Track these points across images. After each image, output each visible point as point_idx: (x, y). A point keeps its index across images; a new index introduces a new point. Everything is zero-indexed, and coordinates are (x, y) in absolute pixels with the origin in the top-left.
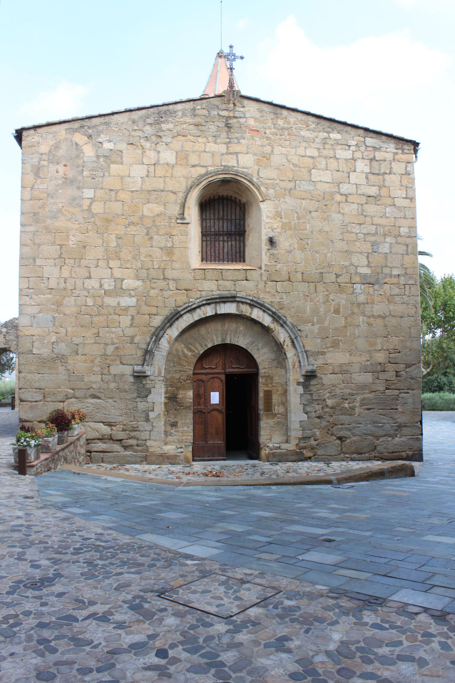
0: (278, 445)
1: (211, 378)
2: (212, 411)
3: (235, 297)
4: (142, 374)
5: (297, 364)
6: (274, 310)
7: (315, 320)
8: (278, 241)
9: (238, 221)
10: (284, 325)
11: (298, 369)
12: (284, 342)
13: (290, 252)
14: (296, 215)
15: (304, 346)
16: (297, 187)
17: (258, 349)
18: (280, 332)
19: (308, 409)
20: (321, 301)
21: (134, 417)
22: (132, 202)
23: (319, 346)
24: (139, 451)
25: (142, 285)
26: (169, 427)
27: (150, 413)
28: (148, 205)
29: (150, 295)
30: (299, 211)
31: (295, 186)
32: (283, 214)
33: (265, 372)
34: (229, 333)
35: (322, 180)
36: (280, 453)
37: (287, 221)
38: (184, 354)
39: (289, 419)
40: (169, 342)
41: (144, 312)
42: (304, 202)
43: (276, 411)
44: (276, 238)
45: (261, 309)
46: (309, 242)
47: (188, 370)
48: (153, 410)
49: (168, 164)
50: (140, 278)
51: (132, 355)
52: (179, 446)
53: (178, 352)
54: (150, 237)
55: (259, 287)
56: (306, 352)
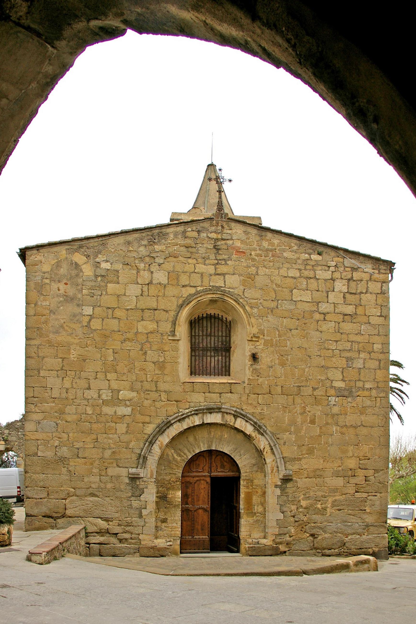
0: (257, 541)
3: (220, 408)
4: (136, 476)
5: (275, 469)
6: (255, 420)
7: (292, 429)
8: (260, 358)
10: (264, 434)
11: (277, 474)
12: (264, 449)
14: (277, 333)
15: (281, 452)
16: (279, 306)
17: (241, 455)
18: (261, 440)
19: (285, 509)
20: (298, 412)
21: (129, 514)
22: (127, 319)
23: (295, 453)
24: (133, 544)
25: (137, 396)
26: (160, 523)
31: (278, 305)
32: (265, 332)
34: (215, 440)
37: (269, 338)
38: (174, 458)
39: (267, 518)
40: (160, 448)
42: (285, 320)
43: (255, 511)
46: (289, 358)
47: (177, 473)
51: (127, 459)
52: (168, 540)
56: (283, 458)
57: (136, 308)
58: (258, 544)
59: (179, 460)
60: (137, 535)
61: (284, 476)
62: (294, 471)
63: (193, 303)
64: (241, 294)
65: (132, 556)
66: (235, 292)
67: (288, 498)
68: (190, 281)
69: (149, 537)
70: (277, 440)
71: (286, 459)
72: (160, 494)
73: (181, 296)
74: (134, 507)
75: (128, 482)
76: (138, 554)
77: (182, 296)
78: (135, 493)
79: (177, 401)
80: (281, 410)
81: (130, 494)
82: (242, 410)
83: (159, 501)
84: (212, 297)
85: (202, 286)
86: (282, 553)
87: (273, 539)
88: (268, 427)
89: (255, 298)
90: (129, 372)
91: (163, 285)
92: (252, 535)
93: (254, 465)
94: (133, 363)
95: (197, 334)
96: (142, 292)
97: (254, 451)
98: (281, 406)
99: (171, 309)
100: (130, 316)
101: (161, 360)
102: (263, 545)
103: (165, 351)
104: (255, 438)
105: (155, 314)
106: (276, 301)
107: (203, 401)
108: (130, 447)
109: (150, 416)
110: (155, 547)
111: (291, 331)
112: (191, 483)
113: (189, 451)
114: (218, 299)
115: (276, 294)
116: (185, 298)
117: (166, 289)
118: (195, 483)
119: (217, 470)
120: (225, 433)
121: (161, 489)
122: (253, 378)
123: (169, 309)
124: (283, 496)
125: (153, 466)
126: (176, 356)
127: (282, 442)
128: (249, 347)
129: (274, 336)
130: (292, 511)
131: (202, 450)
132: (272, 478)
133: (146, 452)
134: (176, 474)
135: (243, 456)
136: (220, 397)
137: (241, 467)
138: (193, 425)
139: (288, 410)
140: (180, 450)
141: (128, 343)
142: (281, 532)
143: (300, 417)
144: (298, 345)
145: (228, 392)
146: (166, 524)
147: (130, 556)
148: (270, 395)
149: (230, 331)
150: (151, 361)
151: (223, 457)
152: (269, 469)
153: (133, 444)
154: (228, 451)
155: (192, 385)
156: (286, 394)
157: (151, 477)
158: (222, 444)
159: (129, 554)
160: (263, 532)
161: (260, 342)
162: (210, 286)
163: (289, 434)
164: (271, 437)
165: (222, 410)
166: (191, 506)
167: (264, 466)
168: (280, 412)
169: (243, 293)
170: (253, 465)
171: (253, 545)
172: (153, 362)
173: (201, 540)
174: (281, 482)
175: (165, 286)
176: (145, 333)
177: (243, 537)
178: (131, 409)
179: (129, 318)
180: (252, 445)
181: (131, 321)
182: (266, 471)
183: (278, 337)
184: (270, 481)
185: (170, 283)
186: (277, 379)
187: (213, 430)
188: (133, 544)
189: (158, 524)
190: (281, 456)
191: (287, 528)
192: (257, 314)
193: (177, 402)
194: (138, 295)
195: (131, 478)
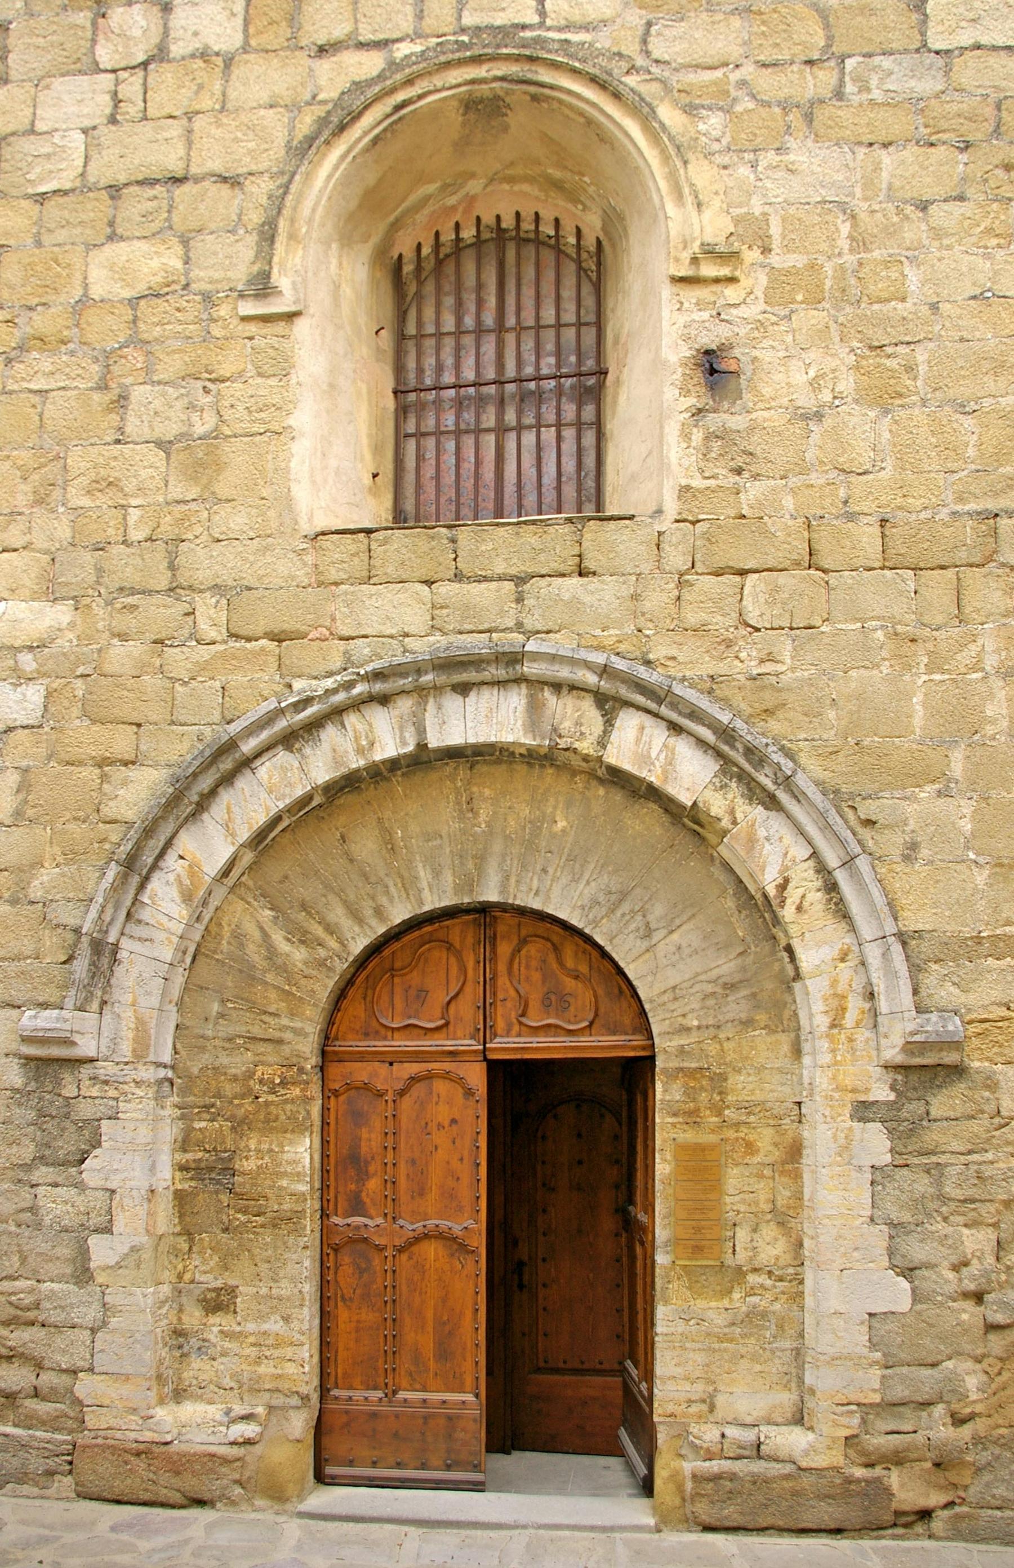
0: (749, 1436)
1: (414, 1080)
2: (417, 1240)
3: (514, 658)
4: (56, 1052)
5: (855, 1005)
6: (725, 718)
7: (957, 767)
8: (748, 369)
9: (569, 335)
10: (783, 796)
11: (864, 1035)
12: (783, 887)
13: (819, 416)
14: (845, 229)
15: (891, 905)
16: (850, 88)
17: (648, 932)
18: (762, 833)
19: (917, 1251)
20: (990, 662)
21: (23, 1260)
22: (39, 244)
23: (981, 905)
24: (43, 1423)
25: (72, 625)
26: (198, 1313)
27: (93, 1241)
28: (110, 250)
29: (108, 668)
30: (861, 207)
31: (841, 83)
32: (775, 229)
33: (681, 1051)
34: (497, 847)
35: (984, 40)
36: (756, 1480)
37: (797, 260)
38: (271, 952)
39: (809, 1301)
40: (187, 897)
41: (75, 752)
42: (886, 158)
43: (742, 1257)
44: (737, 352)
45: (656, 715)
46: (921, 356)
47: (288, 1036)
48: (107, 1229)
49: (204, 55)
50: (64, 592)
51: (18, 958)
52: (239, 1409)
53: (242, 946)
54: (113, 395)
55: (647, 606)
56: (902, 938)
57: (84, 187)
58: (760, 1457)
59: (300, 965)
60: (64, 1377)
61: (909, 1048)
62: (974, 1016)
63: (368, 120)
64: (631, 48)
65: (36, 1491)
66: (598, 45)
67: (939, 1183)
68: (356, 21)
69: (125, 1390)
70: (859, 829)
71: (925, 948)
72: (200, 1155)
73: (308, 97)
74: (47, 1221)
75: (18, 1082)
76: (68, 1480)
77: (314, 97)
78: (54, 1144)
79: (278, 638)
80: (884, 653)
81: (27, 1151)
82: (648, 663)
83: (193, 1193)
84: (468, 77)
85: (418, 35)
86: (904, 1520)
87: (848, 1432)
88: (803, 759)
89: (709, 61)
90: (40, 501)
91: (219, 61)
92: (720, 1400)
93: (731, 987)
94: (58, 457)
95: (430, 329)
96: (116, 106)
97: (730, 903)
98: (880, 634)
99: (254, 168)
100: (52, 226)
101: (199, 430)
102: (789, 1468)
103: (223, 381)
104: (725, 823)
105: (177, 200)
106: (832, 63)
107: (423, 629)
108: (32, 896)
109: (139, 725)
110: (156, 1449)
111: (924, 209)
112: (380, 1094)
113: (359, 920)
114: (505, 85)
115: (827, 26)
116: (330, 106)
117: (233, 77)
118: (402, 1093)
119: (521, 1023)
120: (555, 808)
121: (203, 1124)
122: (712, 482)
123: (245, 170)
124: (905, 1171)
125: (148, 993)
126: (276, 399)
127: (892, 843)
128: (682, 319)
129: (824, 247)
130: (966, 1264)
131: (427, 908)
132: (836, 1063)
133: (107, 918)
134: (280, 1042)
135: (662, 933)
136: (520, 600)
137: (651, 1001)
138: (362, 763)
139: (929, 654)
140: (304, 907)
141: (42, 361)
142: (900, 1392)
143: (1001, 695)
144: (974, 284)
145: (563, 568)
146: (230, 1316)
147: (26, 1489)
148: (812, 572)
149: (598, 288)
150: (148, 437)
151: (556, 948)
152: (818, 1007)
153: (45, 878)
154: (574, 908)
155: (364, 547)
156: (910, 561)
157: (140, 1055)
158: (539, 867)
159: (22, 1478)
160: (786, 1387)
161: (745, 282)
162: (463, 30)
163: (939, 793)
164: (823, 815)
165: (529, 669)
166: (380, 1220)
167: (790, 989)
168: (877, 666)
169: (645, 42)
170: (725, 986)
171: (727, 1465)
172: (159, 444)
173: (433, 1416)
174: (893, 1088)
175: (229, 62)
176: (121, 301)
177: (670, 1408)
178: (43, 693)
179: (47, 239)
180: (717, 871)
181: (56, 249)
182: (804, 1022)
183: (851, 250)
184: (823, 1081)
185: (253, 42)
186: (853, 478)
187: (487, 792)
188: (44, 1423)
189: (185, 1319)
190: (890, 928)
191: (934, 1365)
192: (724, 142)
193: (280, 641)
194: (97, 121)
195: (32, 1064)
